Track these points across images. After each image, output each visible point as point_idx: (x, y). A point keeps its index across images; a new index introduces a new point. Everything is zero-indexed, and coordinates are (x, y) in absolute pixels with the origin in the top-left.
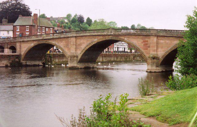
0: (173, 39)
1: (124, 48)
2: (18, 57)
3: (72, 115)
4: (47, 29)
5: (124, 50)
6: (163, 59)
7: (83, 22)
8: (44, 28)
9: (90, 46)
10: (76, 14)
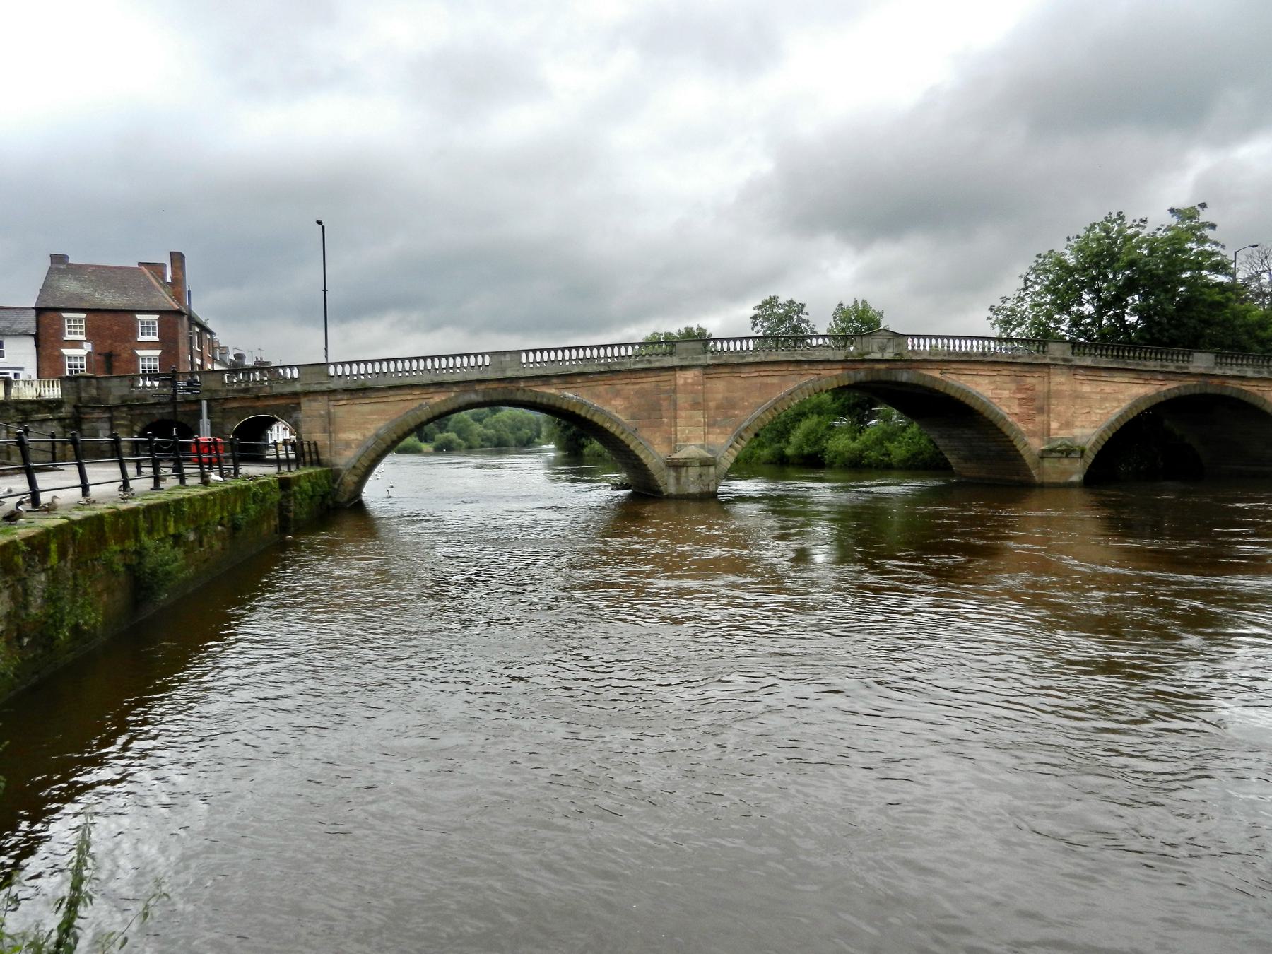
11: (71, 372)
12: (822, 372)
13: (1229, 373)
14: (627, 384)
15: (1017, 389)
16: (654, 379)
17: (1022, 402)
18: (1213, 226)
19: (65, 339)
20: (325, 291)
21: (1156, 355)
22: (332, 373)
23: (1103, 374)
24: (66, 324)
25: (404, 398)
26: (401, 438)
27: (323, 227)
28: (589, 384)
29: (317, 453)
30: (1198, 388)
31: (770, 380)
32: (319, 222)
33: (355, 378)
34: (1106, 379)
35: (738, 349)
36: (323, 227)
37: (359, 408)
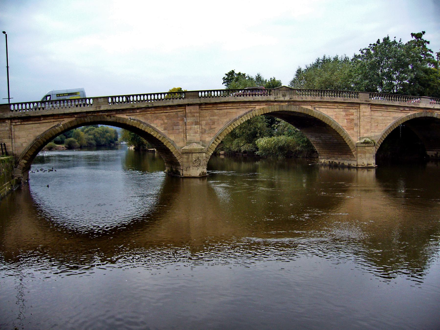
13: (436, 107)
15: (346, 115)
16: (175, 110)
17: (349, 120)
18: (428, 43)
20: (8, 67)
21: (405, 99)
22: (12, 109)
23: (383, 108)
25: (37, 122)
26: (45, 143)
27: (6, 35)
28: (143, 113)
29: (5, 149)
30: (423, 114)
31: (231, 111)
32: (4, 32)
33: (24, 111)
34: (384, 110)
35: (216, 95)
36: (6, 35)
37: (27, 126)
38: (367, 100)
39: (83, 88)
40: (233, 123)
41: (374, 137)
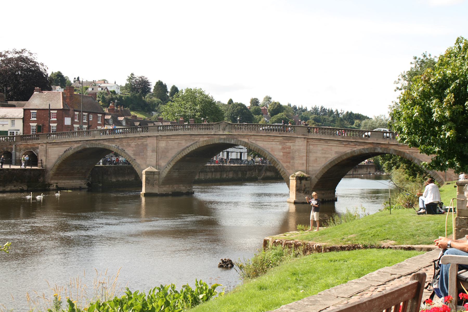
0: (335, 145)
1: (239, 154)
2: (43, 172)
3: (395, 91)
4: (91, 116)
5: (239, 157)
6: (317, 180)
7: (149, 91)
8: (86, 114)
9: (184, 154)
10: (132, 74)
11: (52, 132)
12: (200, 139)
14: (132, 142)
15: (282, 148)
19: (31, 120)
24: (52, 115)
38: (304, 134)
39: (295, 106)
40: (182, 153)
41: (312, 171)
